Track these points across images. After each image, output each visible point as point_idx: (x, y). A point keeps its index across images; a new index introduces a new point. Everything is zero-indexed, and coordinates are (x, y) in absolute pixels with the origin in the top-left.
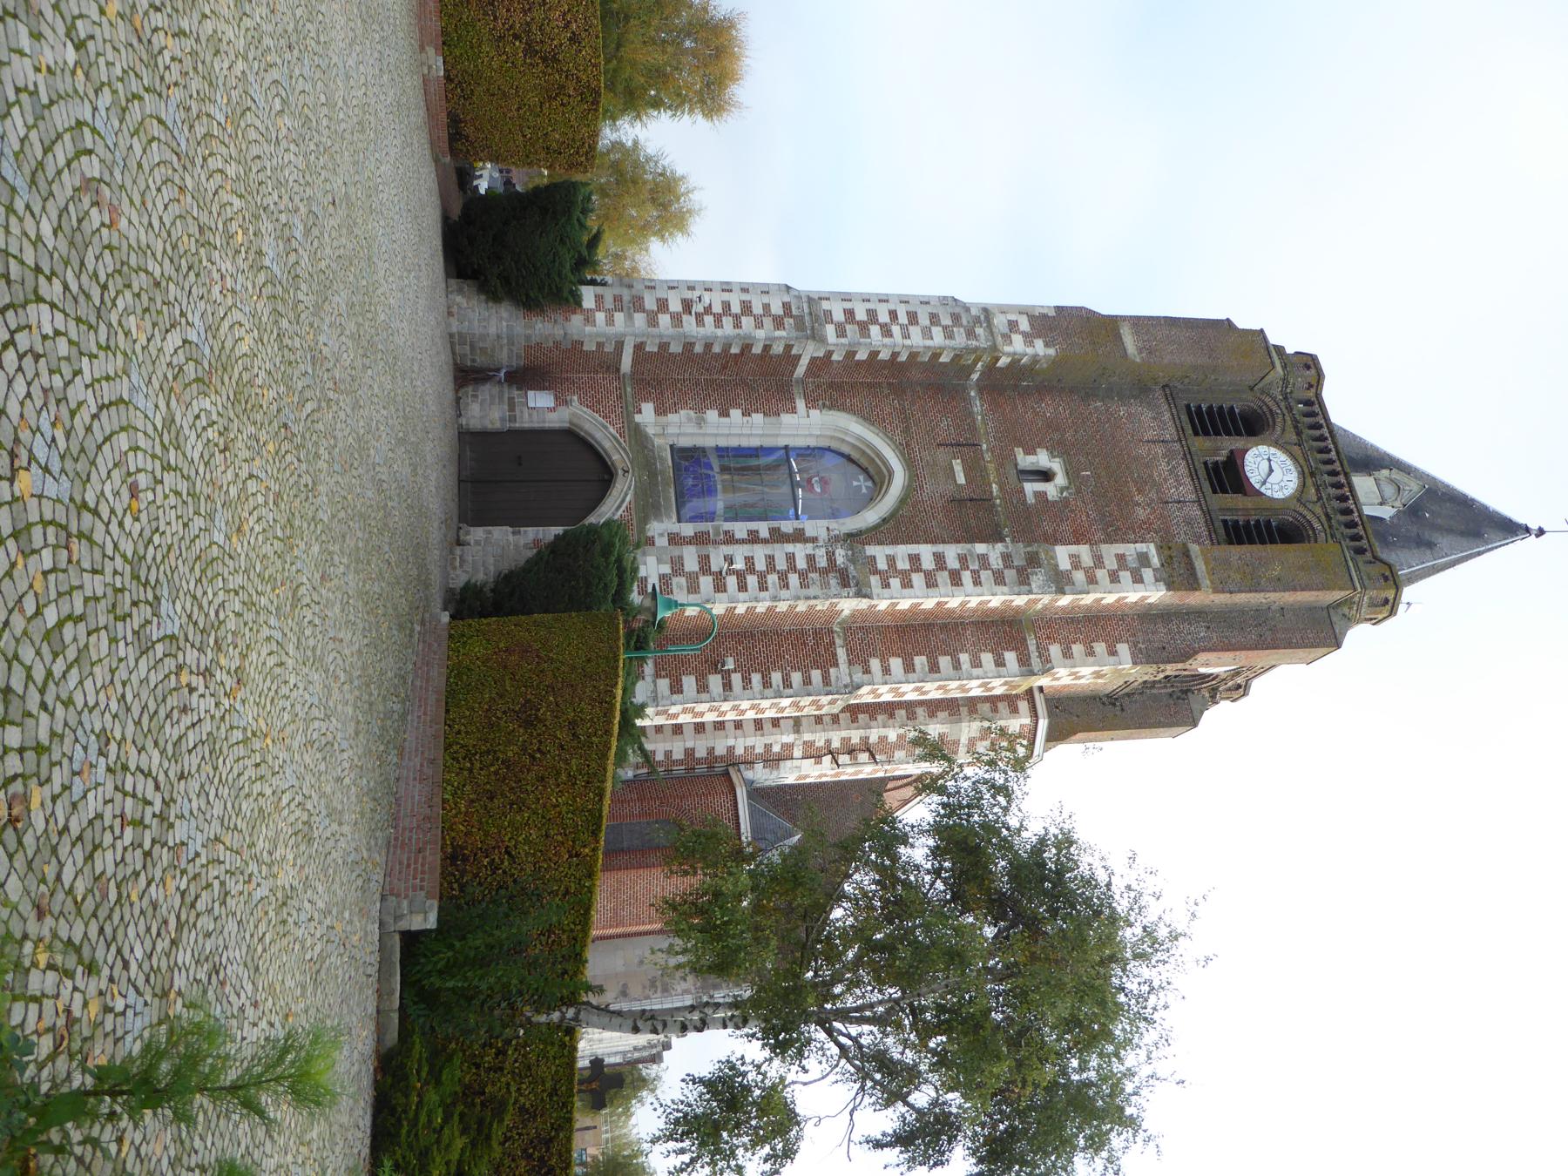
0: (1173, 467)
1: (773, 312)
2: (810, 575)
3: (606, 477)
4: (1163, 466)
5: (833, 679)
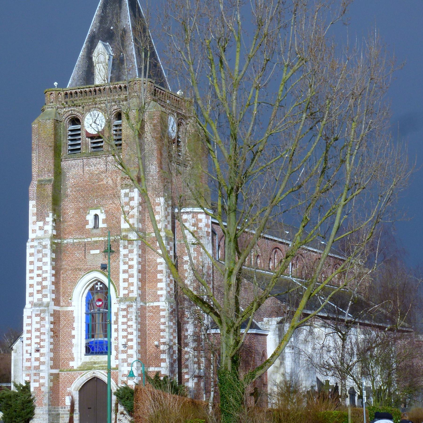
0: (93, 164)
1: (39, 320)
2: (129, 318)
3: (95, 379)
4: (93, 168)
5: (163, 308)
